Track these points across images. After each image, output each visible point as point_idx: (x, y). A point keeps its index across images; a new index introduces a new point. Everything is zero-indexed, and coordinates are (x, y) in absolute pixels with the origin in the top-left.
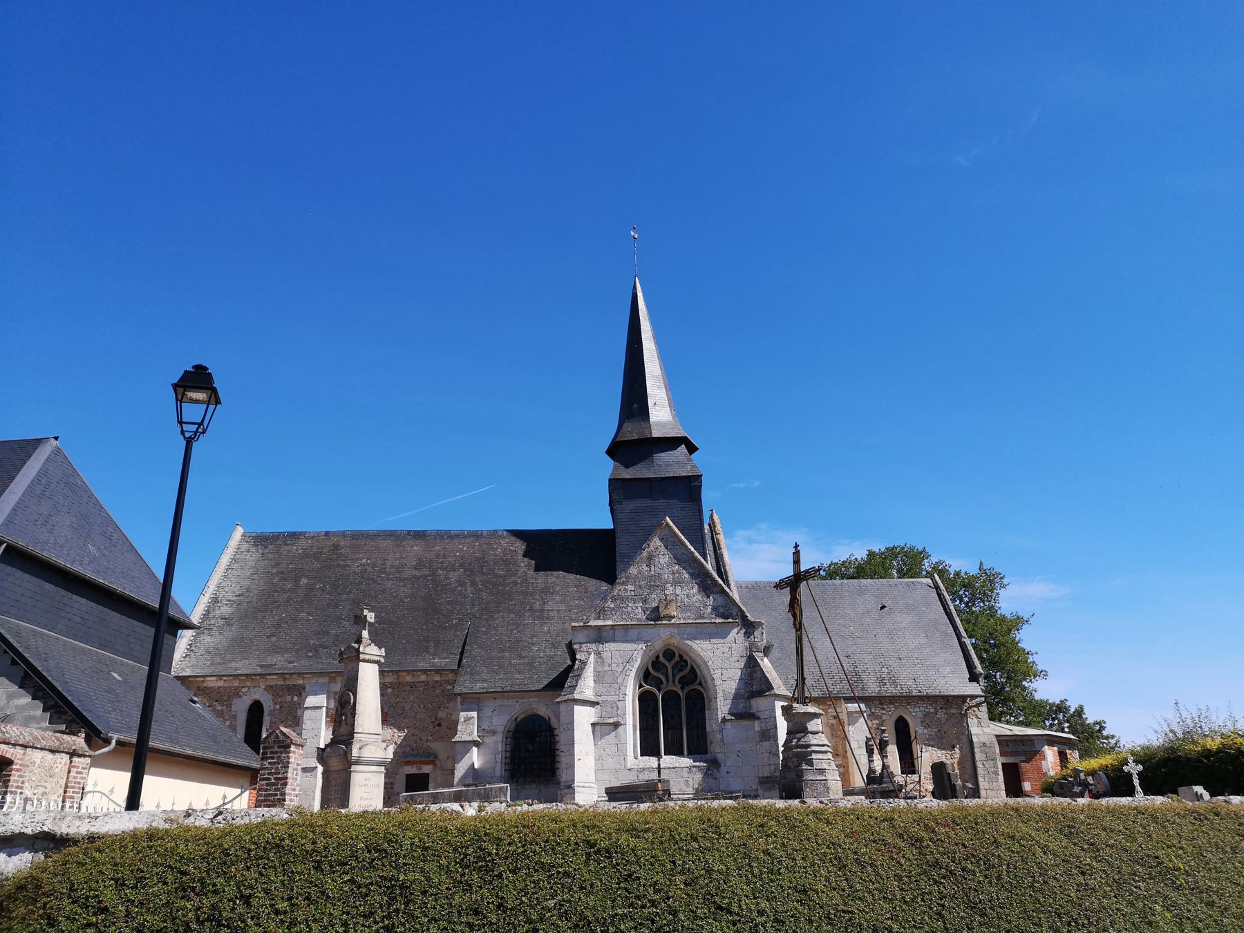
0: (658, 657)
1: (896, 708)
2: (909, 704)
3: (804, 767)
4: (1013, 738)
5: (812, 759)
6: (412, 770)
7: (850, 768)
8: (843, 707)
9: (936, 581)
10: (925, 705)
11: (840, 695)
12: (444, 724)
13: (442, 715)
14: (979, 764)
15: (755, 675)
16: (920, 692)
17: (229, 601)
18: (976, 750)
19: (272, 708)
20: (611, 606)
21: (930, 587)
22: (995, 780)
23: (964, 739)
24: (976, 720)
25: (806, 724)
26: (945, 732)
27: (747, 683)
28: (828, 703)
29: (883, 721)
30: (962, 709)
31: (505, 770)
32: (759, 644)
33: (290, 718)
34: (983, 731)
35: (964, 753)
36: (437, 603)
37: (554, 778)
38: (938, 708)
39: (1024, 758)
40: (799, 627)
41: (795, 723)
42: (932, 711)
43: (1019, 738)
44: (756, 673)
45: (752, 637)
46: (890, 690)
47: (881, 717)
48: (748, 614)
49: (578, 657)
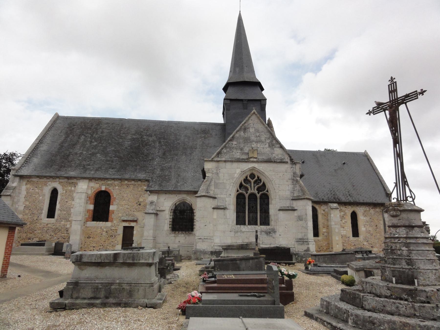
0: (247, 177)
6: (127, 224)
12: (142, 204)
13: (141, 200)
17: (48, 143)
19: (62, 192)
20: (224, 151)
27: (291, 192)
31: (170, 227)
33: (70, 197)
36: (142, 150)
37: (193, 232)
40: (397, 141)
49: (207, 175)
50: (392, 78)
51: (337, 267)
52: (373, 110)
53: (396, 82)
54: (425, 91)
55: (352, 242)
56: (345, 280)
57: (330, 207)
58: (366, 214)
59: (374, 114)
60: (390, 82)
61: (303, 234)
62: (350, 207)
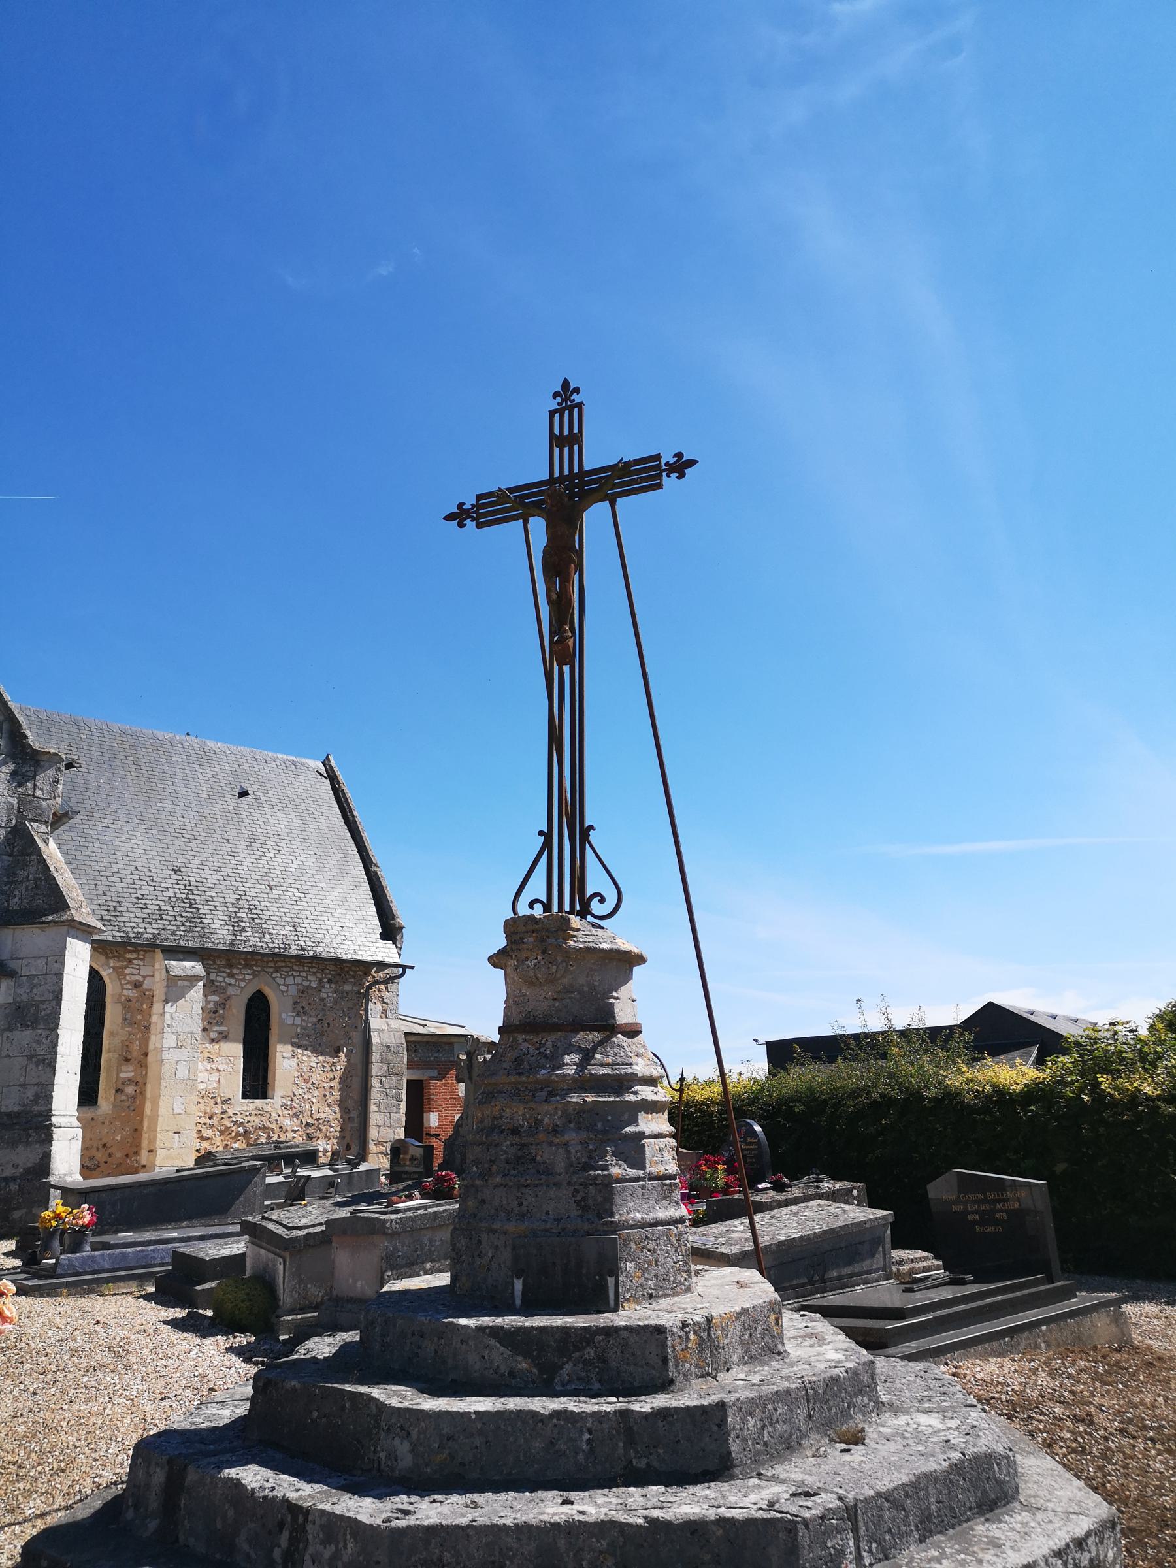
1: (255, 974)
2: (277, 970)
3: (615, 1171)
4: (426, 1038)
5: (641, 1136)
7: (149, 1087)
8: (157, 966)
9: (331, 766)
10: (304, 974)
11: (158, 942)
14: (375, 1083)
15: (22, 874)
16: (303, 949)
18: (375, 1057)
21: (321, 775)
22: (395, 1110)
23: (357, 1037)
24: (379, 1005)
25: (607, 994)
26: (328, 1024)
28: (128, 956)
29: (228, 999)
30: (361, 986)
32: (44, 804)
34: (388, 1025)
35: (352, 1061)
38: (325, 980)
39: (435, 1073)
41: (568, 990)
42: (314, 985)
43: (435, 1039)
44: (25, 866)
45: (29, 785)
46: (252, 941)
47: (224, 990)
48: (28, 733)
50: (566, 384)
51: (189, 1239)
52: (477, 506)
53: (580, 406)
54: (692, 463)
55: (235, 1123)
56: (851, 1496)
57: (167, 972)
58: (304, 1004)
59: (479, 526)
60: (559, 399)
61: (30, 1093)
62: (247, 974)
